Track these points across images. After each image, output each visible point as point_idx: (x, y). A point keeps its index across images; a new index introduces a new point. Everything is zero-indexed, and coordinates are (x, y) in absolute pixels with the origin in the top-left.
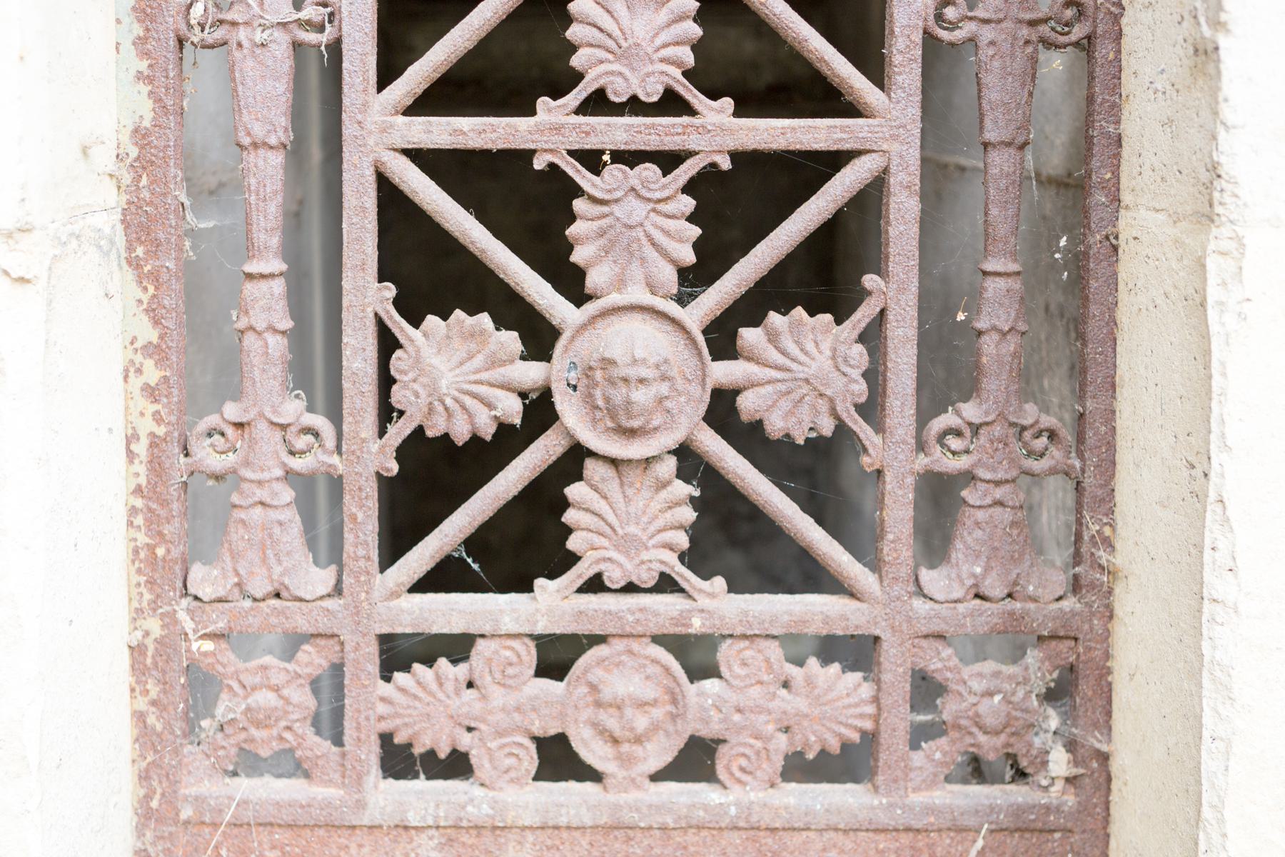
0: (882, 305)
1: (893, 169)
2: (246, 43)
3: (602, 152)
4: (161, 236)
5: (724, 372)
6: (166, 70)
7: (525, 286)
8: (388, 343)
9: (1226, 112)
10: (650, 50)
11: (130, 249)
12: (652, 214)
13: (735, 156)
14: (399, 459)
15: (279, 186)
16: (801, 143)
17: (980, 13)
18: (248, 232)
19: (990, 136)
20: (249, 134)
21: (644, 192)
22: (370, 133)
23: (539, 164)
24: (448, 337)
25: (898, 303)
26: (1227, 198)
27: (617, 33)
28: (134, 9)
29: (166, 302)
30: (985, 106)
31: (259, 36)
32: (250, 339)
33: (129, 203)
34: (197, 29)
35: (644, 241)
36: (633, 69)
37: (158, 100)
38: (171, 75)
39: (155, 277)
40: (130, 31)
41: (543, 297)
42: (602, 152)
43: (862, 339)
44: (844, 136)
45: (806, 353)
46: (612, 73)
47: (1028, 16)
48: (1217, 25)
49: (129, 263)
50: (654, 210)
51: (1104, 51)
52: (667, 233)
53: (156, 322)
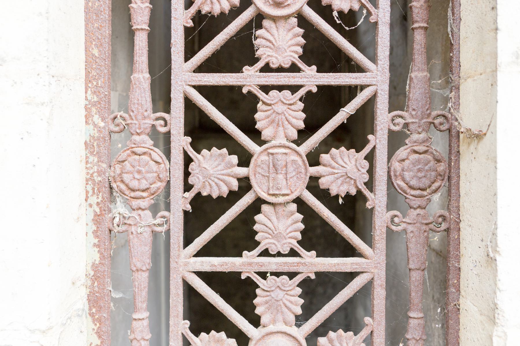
0: (372, 330)
1: (375, 279)
2: (134, 232)
3: (267, 273)
4: (102, 305)
5: (314, 170)
6: (105, 242)
7: (238, 323)
8: (188, 160)
9: (499, 284)
10: (285, 234)
11: (90, 309)
12: (286, 295)
13: (316, 274)
14: (191, 203)
15: (146, 285)
16: (341, 269)
17: (407, 220)
18: (135, 302)
19: (412, 266)
20: (135, 266)
21: (283, 288)
22: (181, 266)
23: (243, 277)
24: (209, 341)
25: (377, 329)
26: (500, 317)
27: (273, 228)
28: (93, 220)
29: (103, 329)
30: (410, 255)
31: (139, 230)
32: (135, 342)
33: (90, 292)
34: (116, 227)
35: (283, 306)
36: (278, 241)
37: (101, 254)
38: (107, 244)
39: (99, 320)
40: (91, 228)
41: (245, 327)
42: (267, 273)
43: (366, 158)
44: (357, 267)
45: (346, 163)
46: (271, 243)
47: (425, 222)
48: (495, 251)
49: (90, 314)
50: (286, 294)
51: (453, 235)
52: (291, 302)
53: (100, 337)
